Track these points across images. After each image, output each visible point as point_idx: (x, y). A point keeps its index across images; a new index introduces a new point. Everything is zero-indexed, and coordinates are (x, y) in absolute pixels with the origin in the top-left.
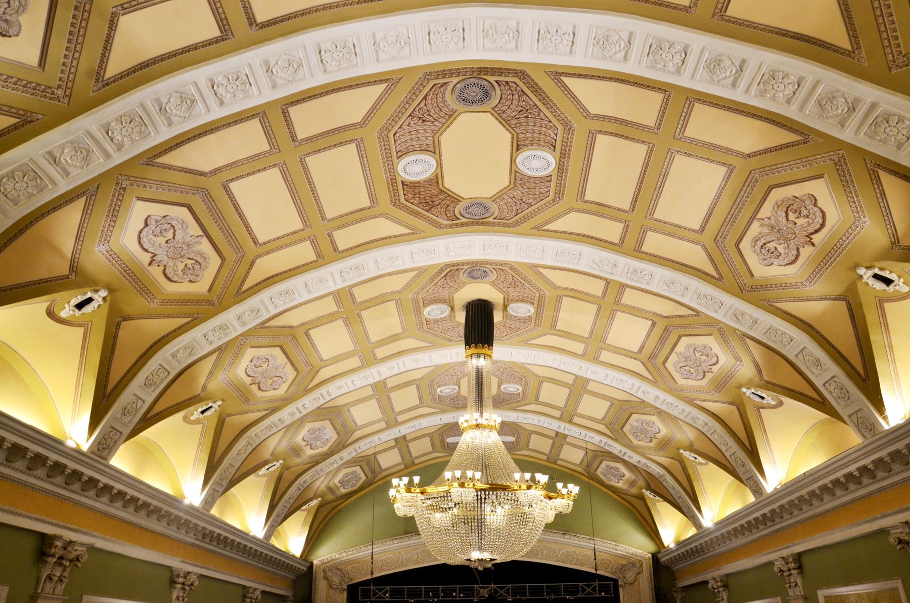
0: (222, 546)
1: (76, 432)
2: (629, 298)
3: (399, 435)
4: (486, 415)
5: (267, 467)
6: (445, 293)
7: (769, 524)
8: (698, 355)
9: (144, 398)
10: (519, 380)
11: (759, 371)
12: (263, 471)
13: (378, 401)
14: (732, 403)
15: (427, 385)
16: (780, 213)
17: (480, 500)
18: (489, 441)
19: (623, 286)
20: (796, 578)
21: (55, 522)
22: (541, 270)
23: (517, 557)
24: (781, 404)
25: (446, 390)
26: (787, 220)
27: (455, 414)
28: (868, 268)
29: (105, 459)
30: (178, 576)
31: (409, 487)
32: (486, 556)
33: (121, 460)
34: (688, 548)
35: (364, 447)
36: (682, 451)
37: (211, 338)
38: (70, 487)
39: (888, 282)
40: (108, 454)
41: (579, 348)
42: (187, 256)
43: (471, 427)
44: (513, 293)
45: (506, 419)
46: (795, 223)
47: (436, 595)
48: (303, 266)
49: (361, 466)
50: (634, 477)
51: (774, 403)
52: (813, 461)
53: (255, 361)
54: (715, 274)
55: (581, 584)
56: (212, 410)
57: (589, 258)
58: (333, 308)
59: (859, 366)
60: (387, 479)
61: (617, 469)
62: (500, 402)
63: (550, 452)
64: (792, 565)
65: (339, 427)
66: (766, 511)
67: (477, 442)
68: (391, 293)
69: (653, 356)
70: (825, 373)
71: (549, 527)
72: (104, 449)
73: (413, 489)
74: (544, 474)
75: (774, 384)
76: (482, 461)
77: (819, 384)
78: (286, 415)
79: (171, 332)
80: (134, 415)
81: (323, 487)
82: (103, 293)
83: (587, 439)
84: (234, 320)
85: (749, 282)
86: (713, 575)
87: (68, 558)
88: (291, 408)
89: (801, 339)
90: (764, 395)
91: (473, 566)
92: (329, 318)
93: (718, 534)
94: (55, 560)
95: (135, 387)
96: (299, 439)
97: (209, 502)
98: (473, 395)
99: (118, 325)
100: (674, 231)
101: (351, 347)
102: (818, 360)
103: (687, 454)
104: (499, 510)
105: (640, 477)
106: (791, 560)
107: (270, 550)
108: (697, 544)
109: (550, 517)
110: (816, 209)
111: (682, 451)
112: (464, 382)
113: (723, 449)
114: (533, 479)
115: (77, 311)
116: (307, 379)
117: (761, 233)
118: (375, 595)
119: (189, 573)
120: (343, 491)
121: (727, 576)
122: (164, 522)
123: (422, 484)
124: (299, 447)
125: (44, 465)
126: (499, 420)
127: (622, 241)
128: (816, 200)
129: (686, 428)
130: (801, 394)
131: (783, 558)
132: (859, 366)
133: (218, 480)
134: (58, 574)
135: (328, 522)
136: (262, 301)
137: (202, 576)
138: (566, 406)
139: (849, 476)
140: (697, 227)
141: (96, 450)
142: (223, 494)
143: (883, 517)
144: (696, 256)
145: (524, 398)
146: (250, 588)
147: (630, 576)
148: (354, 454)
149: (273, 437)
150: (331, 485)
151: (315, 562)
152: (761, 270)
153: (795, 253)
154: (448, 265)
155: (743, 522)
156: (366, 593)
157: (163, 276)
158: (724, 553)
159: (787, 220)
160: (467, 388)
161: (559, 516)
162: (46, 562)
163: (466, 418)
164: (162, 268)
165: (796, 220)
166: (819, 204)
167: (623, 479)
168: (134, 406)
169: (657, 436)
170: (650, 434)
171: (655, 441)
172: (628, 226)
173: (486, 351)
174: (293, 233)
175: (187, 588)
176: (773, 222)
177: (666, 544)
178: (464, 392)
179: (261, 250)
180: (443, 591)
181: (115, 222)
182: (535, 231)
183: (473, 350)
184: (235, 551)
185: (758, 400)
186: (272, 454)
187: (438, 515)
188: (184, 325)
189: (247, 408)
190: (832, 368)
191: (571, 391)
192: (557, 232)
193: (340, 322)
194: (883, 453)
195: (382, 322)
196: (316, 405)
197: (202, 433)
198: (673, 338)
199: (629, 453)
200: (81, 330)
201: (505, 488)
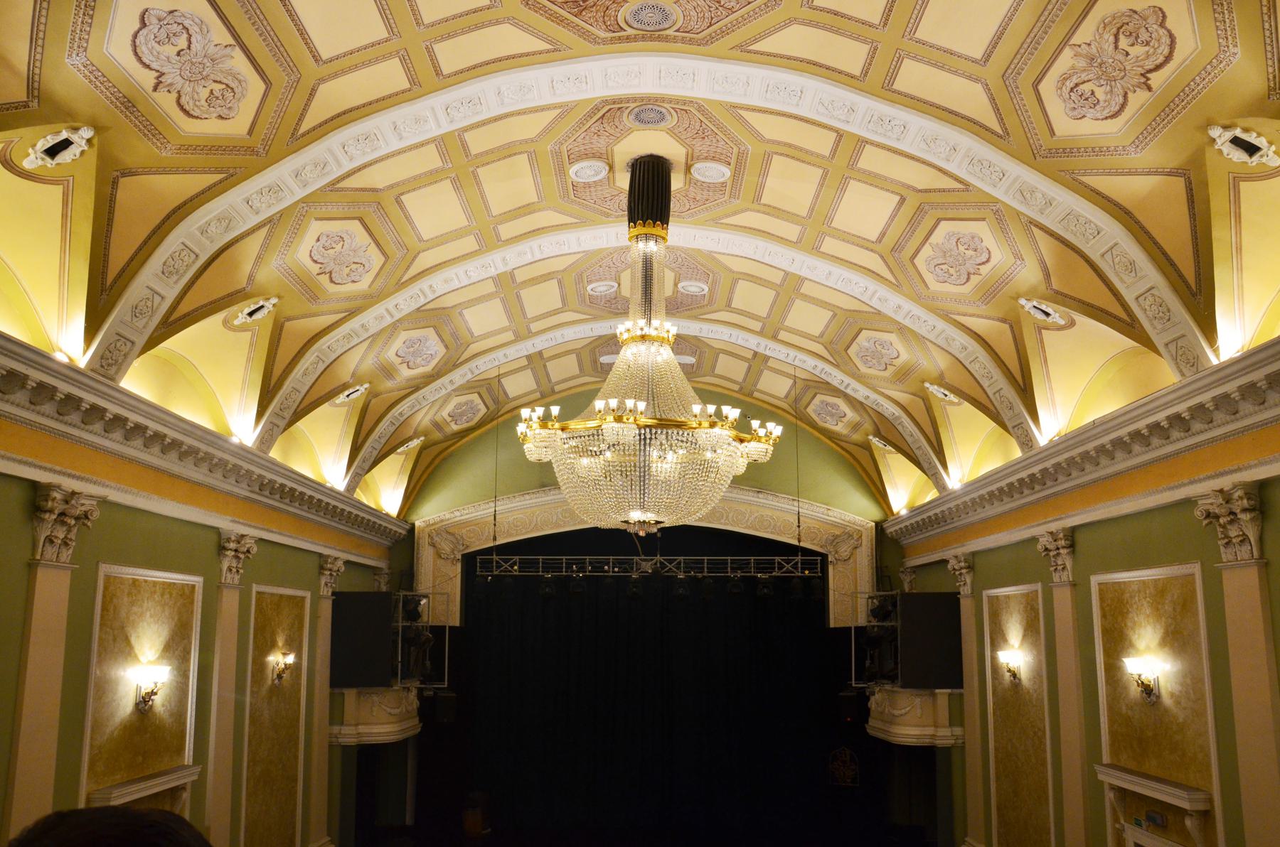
0: (287, 501)
1: (68, 342)
2: (870, 160)
3: (532, 351)
4: (655, 323)
5: (347, 393)
6: (600, 144)
7: (1037, 487)
9: (163, 292)
10: (705, 276)
11: (1047, 275)
12: (341, 398)
13: (503, 300)
14: (1003, 321)
15: (573, 281)
16: (1106, 36)
17: (644, 441)
18: (659, 359)
19: (863, 142)
20: (1066, 559)
21: (49, 466)
23: (691, 521)
24: (1072, 323)
25: (601, 288)
26: (1116, 48)
27: (611, 322)
28: (1225, 128)
29: (112, 379)
30: (229, 540)
31: (545, 420)
32: (650, 517)
33: (137, 381)
34: (925, 516)
35: (484, 367)
36: (927, 385)
37: (256, 204)
38: (66, 418)
39: (1251, 149)
40: (117, 373)
41: (792, 231)
42: (212, 76)
43: (633, 339)
44: (700, 147)
45: (684, 332)
46: (1127, 54)
47: (582, 569)
48: (390, 96)
50: (858, 418)
51: (1062, 322)
52: (1108, 405)
53: (323, 239)
54: (998, 130)
55: (777, 559)
56: (265, 311)
57: (815, 96)
58: (437, 163)
59: (1190, 275)
60: (515, 413)
61: (834, 406)
62: (676, 307)
63: (745, 380)
64: (1063, 543)
65: (447, 337)
66: (1036, 470)
67: (641, 360)
68: (521, 142)
69: (897, 248)
70: (1141, 282)
71: (737, 482)
72: (109, 365)
73: (550, 424)
74: (734, 407)
75: (1066, 296)
76: (648, 386)
77: (1129, 297)
78: (373, 318)
79: (191, 199)
81: (426, 422)
82: (87, 133)
83: (796, 363)
84: (289, 178)
85: (1045, 141)
86: (954, 553)
87: (73, 516)
88: (379, 309)
89: (1113, 231)
90: (1049, 310)
91: (631, 530)
92: (431, 178)
93: (967, 499)
94: (54, 517)
95: (148, 275)
96: (390, 354)
97: (266, 440)
98: (638, 296)
99: (115, 183)
100: (944, 59)
101: (463, 222)
102: (1132, 263)
103: (935, 390)
104: (670, 456)
105: (866, 416)
106: (1061, 535)
107: (354, 506)
108: (938, 511)
109: (741, 467)
110: (1162, 31)
111: (927, 385)
112: (626, 277)
113: (985, 384)
114: (718, 414)
115: (48, 159)
116: (399, 270)
117: (1073, 68)
119: (243, 536)
120: (455, 428)
121: (974, 554)
122: (204, 468)
123: (561, 418)
124: (392, 365)
125: (23, 387)
126: (674, 330)
127: (865, 72)
128: (1164, 16)
129: (935, 352)
130: (1102, 310)
131: (1051, 533)
132: (1190, 275)
133: (277, 410)
134: (61, 536)
135: (432, 473)
136: (330, 151)
137: (261, 540)
138: (769, 315)
139: (1155, 427)
140: (978, 55)
141: (98, 366)
142: (285, 430)
143: (1191, 483)
144: (970, 97)
145: (711, 302)
146: (328, 556)
147: (844, 550)
148: (469, 376)
149: (355, 350)
150: (438, 418)
151: (417, 524)
152: (1066, 125)
153: (1121, 100)
154: (605, 102)
155: (1003, 484)
156: (487, 565)
157: (177, 110)
158: (972, 524)
159: (1116, 48)
160: (630, 286)
161: (753, 466)
162: (43, 520)
163: (624, 328)
164: (175, 95)
165: (1129, 49)
166: (1168, 24)
167: (842, 421)
168: (149, 304)
170: (885, 360)
171: (891, 369)
172: (876, 49)
173: (658, 230)
174: (373, 45)
175: (242, 556)
176: (1094, 50)
177: (895, 510)
178: (626, 292)
179: (325, 70)
180: (590, 563)
181: (92, 17)
182: (737, 53)
183: (640, 230)
184: (305, 508)
185: (1040, 316)
186: (353, 375)
187: (585, 461)
188: (215, 185)
189: (314, 308)
190: (1152, 276)
191: (778, 294)
192: (769, 55)
193: (447, 184)
194: (1205, 398)
195: (508, 185)
196: (415, 306)
197: (251, 345)
198: (928, 222)
199: (855, 384)
200: (58, 190)
201: (680, 425)
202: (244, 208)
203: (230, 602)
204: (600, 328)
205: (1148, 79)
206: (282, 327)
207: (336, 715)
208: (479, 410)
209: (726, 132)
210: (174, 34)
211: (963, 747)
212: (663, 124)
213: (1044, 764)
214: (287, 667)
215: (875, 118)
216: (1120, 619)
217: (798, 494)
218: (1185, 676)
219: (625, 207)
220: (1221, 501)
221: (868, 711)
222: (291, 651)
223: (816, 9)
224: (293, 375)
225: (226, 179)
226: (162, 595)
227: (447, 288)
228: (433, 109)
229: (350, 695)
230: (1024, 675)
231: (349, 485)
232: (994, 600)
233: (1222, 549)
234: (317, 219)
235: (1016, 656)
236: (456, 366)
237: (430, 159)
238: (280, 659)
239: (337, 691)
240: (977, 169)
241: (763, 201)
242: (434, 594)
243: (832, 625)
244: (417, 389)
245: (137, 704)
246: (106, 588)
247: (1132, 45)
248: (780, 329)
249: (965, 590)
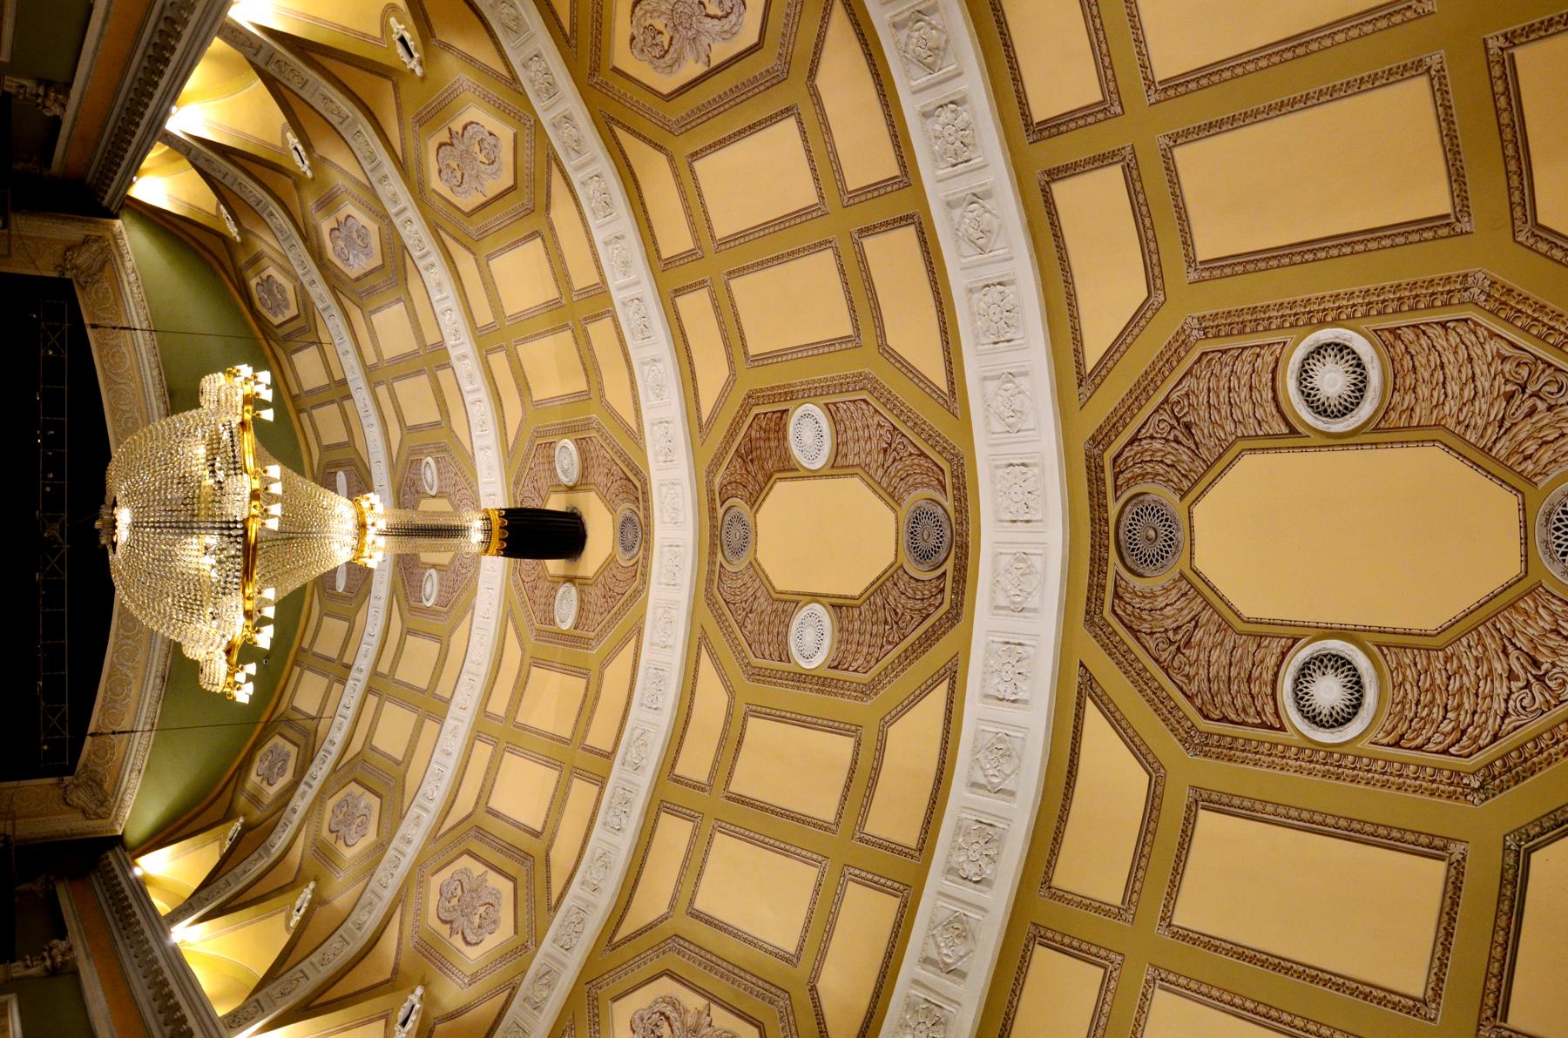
2: (581, 792)
3: (352, 387)
5: (300, 148)
6: (598, 477)
8: (482, 910)
10: (446, 601)
11: (452, 1016)
12: (293, 140)
13: (414, 353)
14: (395, 971)
15: (438, 440)
17: (226, 527)
18: (335, 546)
19: (601, 782)
22: (632, 643)
25: (430, 473)
31: (253, 401)
32: (123, 534)
34: (132, 900)
35: (332, 325)
36: (312, 885)
37: (534, 66)
41: (498, 706)
43: (360, 514)
44: (595, 592)
45: (376, 578)
48: (653, 235)
49: (297, 317)
53: (490, 139)
56: (406, 59)
57: (651, 723)
58: (578, 284)
62: (407, 570)
63: (315, 654)
65: (372, 280)
67: (334, 524)
68: (600, 383)
69: (481, 833)
76: (299, 531)
78: (394, 189)
81: (261, 246)
83: (338, 719)
84: (563, 108)
90: (409, 1025)
91: (104, 510)
92: (561, 274)
98: (420, 521)
101: (509, 310)
103: (307, 894)
104: (210, 560)
109: (193, 652)
111: (312, 885)
112: (443, 505)
113: (314, 958)
114: (264, 621)
117: (686, 1011)
120: (253, 283)
121: (75, 973)
123: (258, 423)
124: (336, 209)
127: (678, 780)
133: (277, 57)
136: (593, 160)
140: (699, 905)
144: (652, 903)
145: (412, 609)
146: (67, 96)
148: (320, 306)
151: (118, 223)
154: (645, 483)
155: (179, 997)
158: (121, 967)
160: (433, 509)
161: (195, 667)
163: (378, 508)
170: (343, 829)
171: (331, 838)
172: (703, 790)
173: (496, 544)
177: (141, 860)
178: (426, 505)
179: (682, 163)
183: (496, 522)
185: (401, 1015)
186: (324, 159)
187: (201, 451)
192: (696, 671)
193: (553, 293)
195: (550, 365)
196: (409, 243)
197: (364, 35)
198: (511, 866)
199: (311, 794)
201: (247, 573)
202: (529, 51)
204: (380, 473)
206: (386, 77)
208: (275, 315)
209: (611, 623)
215: (628, 795)
217: (162, 729)
219: (525, 505)
223: (745, 720)
224: (324, 82)
225: (565, 35)
227: (431, 284)
228: (638, 283)
231: (174, 136)
234: (515, 135)
236: (333, 289)
237: (582, 277)
240: (573, 919)
241: (534, 670)
242: (9, 235)
244: (305, 239)
248: (380, 696)
249: (17, 969)
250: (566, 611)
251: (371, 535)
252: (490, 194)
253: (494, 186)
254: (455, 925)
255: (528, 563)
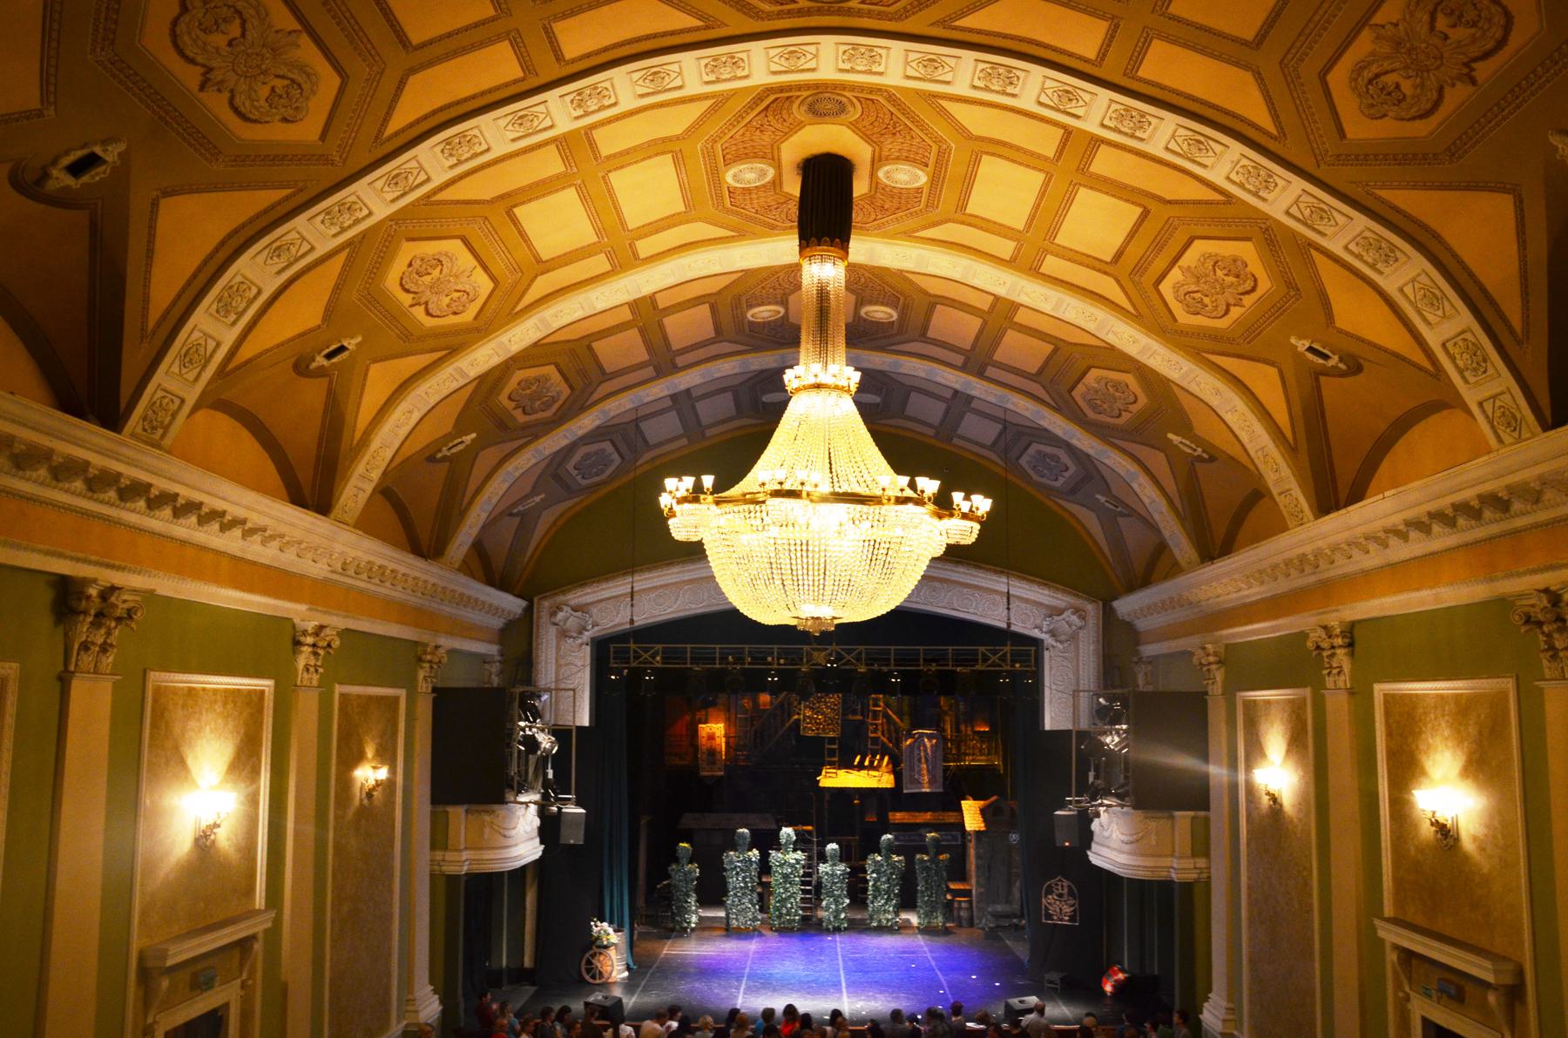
8: (1219, 273)
10: (892, 301)
22: (944, 103)
25: (763, 313)
26: (1432, 28)
46: (1446, 37)
53: (417, 263)
55: (982, 649)
64: (1339, 641)
69: (1139, 269)
74: (932, 478)
80: (204, 367)
87: (108, 608)
94: (90, 619)
110: (1494, 9)
117: (1373, 54)
118: (636, 658)
123: (719, 488)
134: (100, 641)
140: (1249, 35)
153: (1435, 95)
156: (623, 655)
159: (1432, 28)
164: (227, 95)
165: (1450, 32)
169: (1131, 408)
170: (1119, 404)
175: (321, 652)
203: (307, 707)
204: (763, 361)
205: (1473, 70)
207: (439, 839)
210: (225, 20)
211: (1208, 882)
212: (843, 116)
213: (1310, 911)
214: (378, 784)
216: (1410, 740)
218: (1491, 818)
220: (1545, 603)
221: (1091, 833)
222: (383, 763)
226: (225, 704)
229: (457, 813)
230: (1288, 799)
232: (1251, 706)
233: (1545, 663)
234: (409, 240)
235: (1277, 775)
238: (369, 774)
239: (440, 808)
243: (1047, 727)
245: (197, 840)
246: (155, 701)
247: (1454, 26)
249: (1216, 689)
250: (904, 176)
251: (824, 378)
252: (473, 262)
253: (465, 259)
254: (1232, 301)
255: (857, 216)
